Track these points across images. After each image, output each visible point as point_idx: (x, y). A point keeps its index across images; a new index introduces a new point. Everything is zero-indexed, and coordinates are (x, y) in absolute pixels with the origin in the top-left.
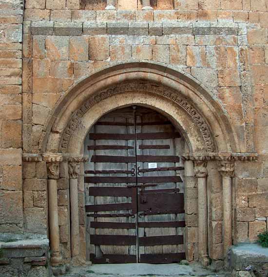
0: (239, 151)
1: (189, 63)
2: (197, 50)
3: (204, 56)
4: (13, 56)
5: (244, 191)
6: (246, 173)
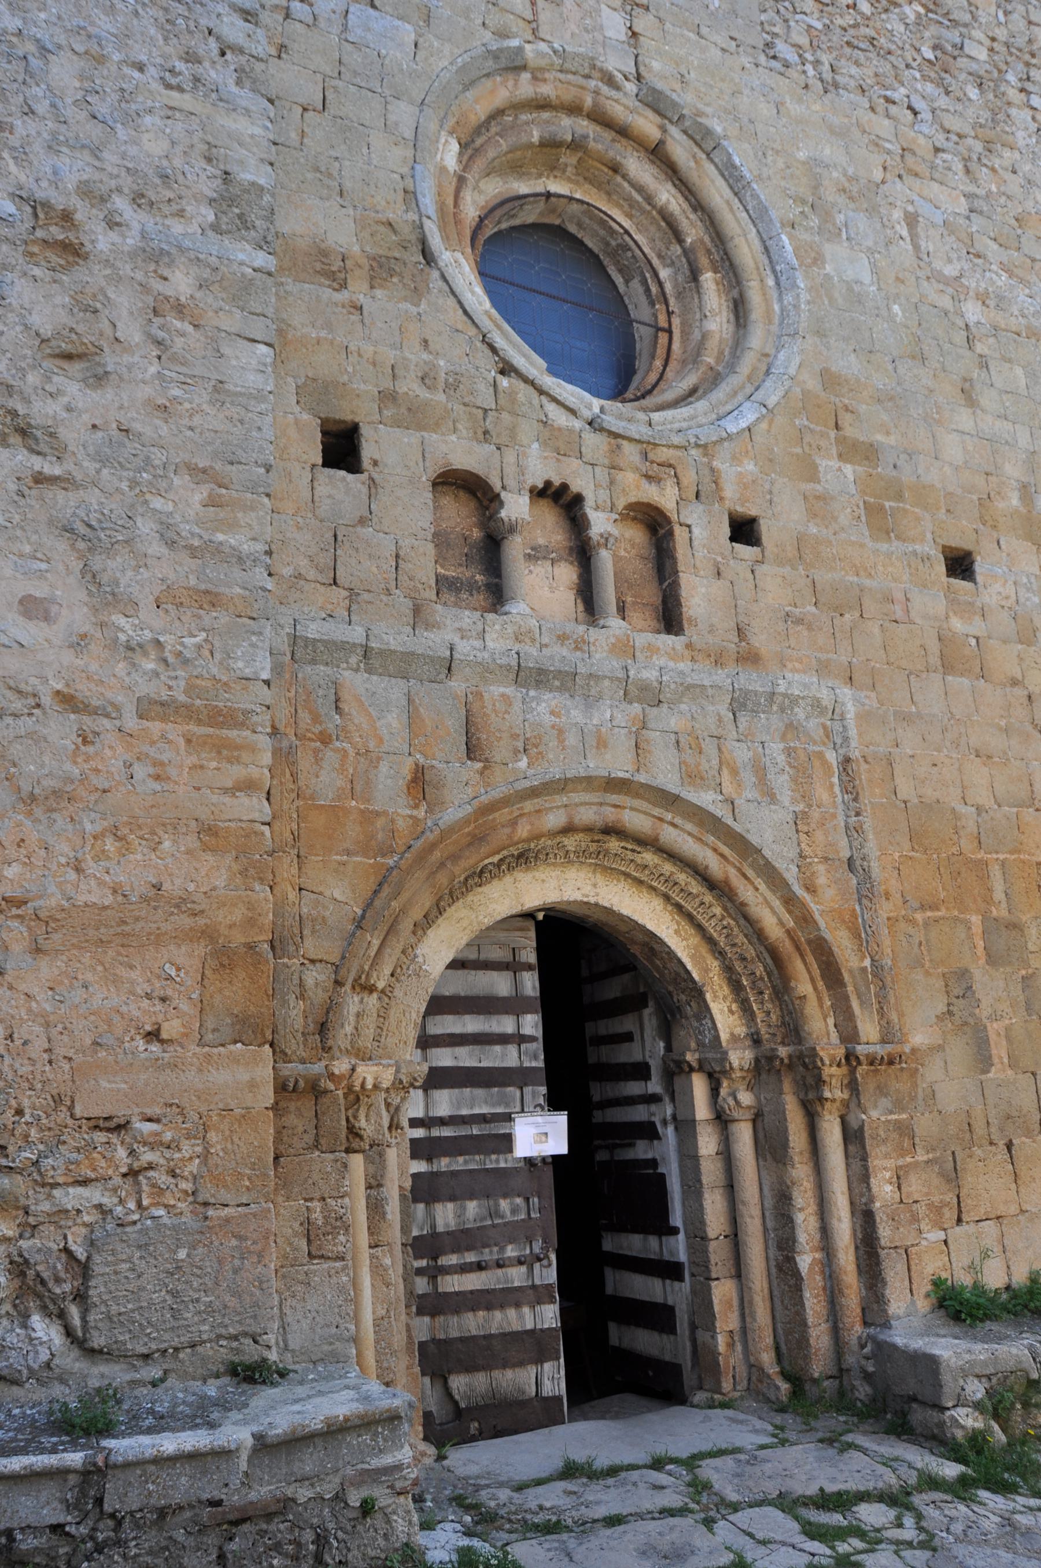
5: (887, 1156)
6: (885, 1102)
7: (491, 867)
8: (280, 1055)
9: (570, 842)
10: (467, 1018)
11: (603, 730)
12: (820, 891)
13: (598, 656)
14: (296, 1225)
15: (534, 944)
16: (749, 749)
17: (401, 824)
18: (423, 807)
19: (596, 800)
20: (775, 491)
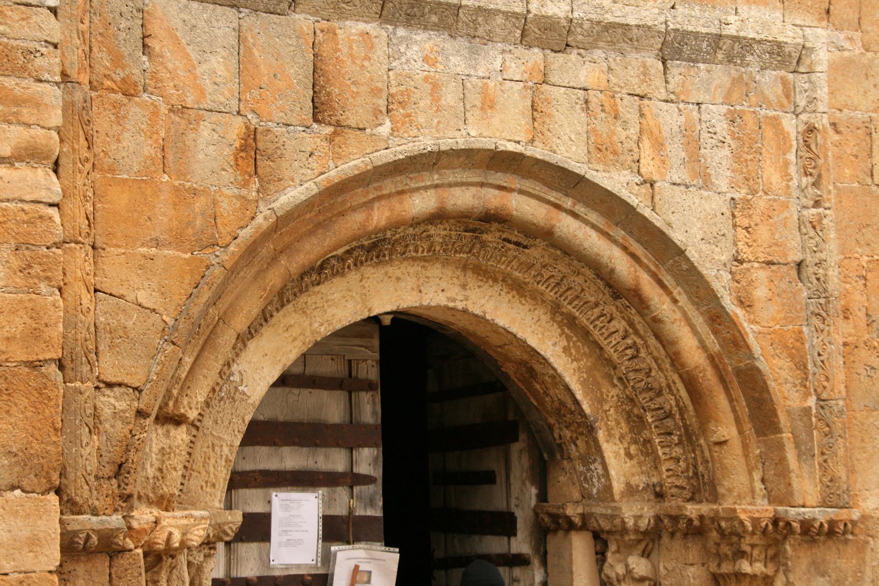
0: (801, 503)
1: (648, 167)
2: (669, 119)
3: (692, 143)
4: (24, 68)
7: (333, 262)
8: (70, 506)
9: (438, 232)
10: (286, 450)
11: (491, 84)
12: (758, 306)
15: (377, 356)
17: (225, 207)
18: (255, 184)
19: (477, 180)
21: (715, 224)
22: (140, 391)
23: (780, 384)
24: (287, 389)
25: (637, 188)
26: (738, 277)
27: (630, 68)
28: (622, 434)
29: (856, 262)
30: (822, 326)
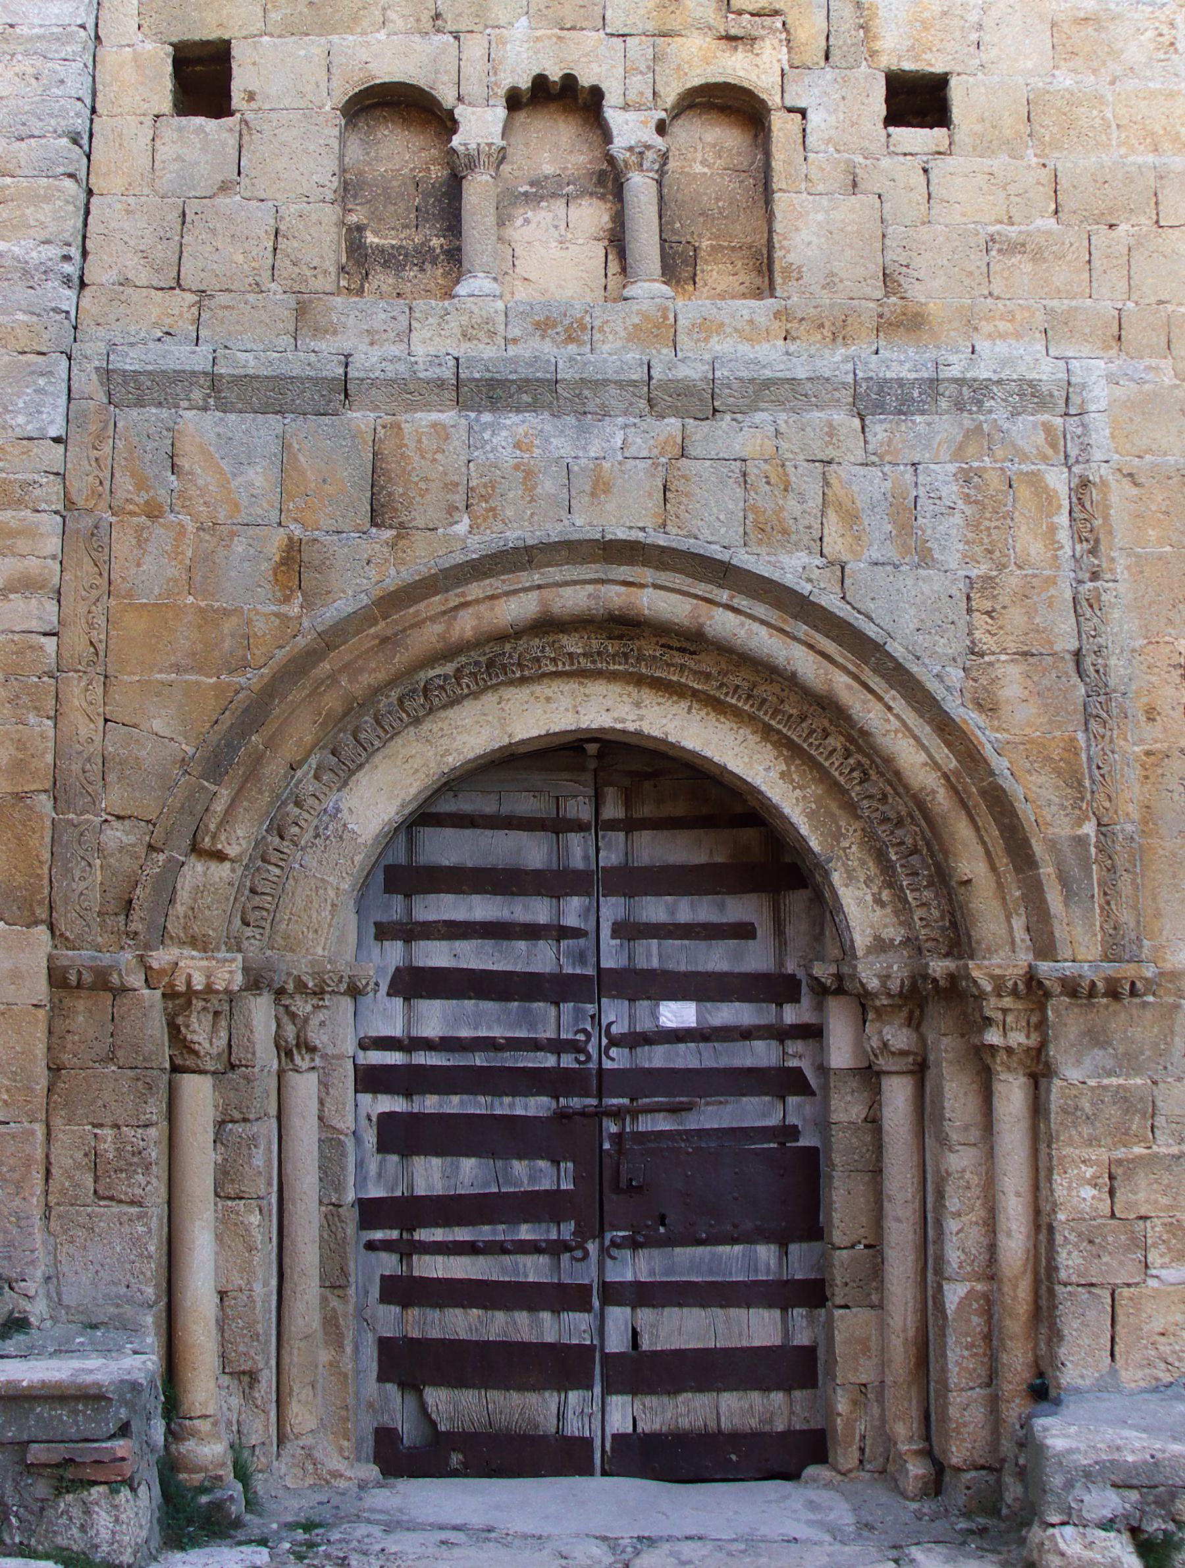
5: (1090, 1142)
10: (476, 899)
11: (606, 465)
12: (1005, 710)
13: (606, 348)
14: (79, 1155)
16: (885, 477)
17: (260, 626)
18: (298, 599)
20: (988, 23)
21: (939, 610)
22: (154, 825)
23: (1039, 807)
24: (479, 831)
25: (817, 571)
26: (974, 674)
27: (809, 429)
28: (868, 877)
29: (1168, 648)
30: (1102, 731)
